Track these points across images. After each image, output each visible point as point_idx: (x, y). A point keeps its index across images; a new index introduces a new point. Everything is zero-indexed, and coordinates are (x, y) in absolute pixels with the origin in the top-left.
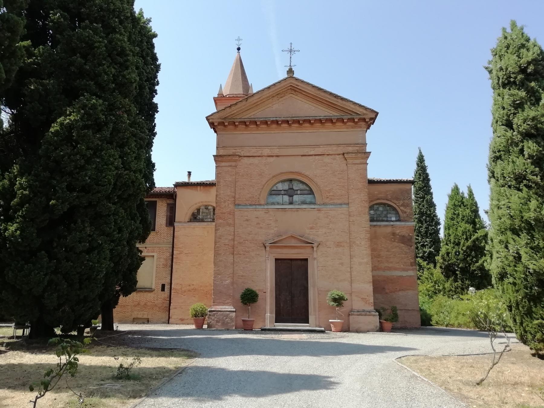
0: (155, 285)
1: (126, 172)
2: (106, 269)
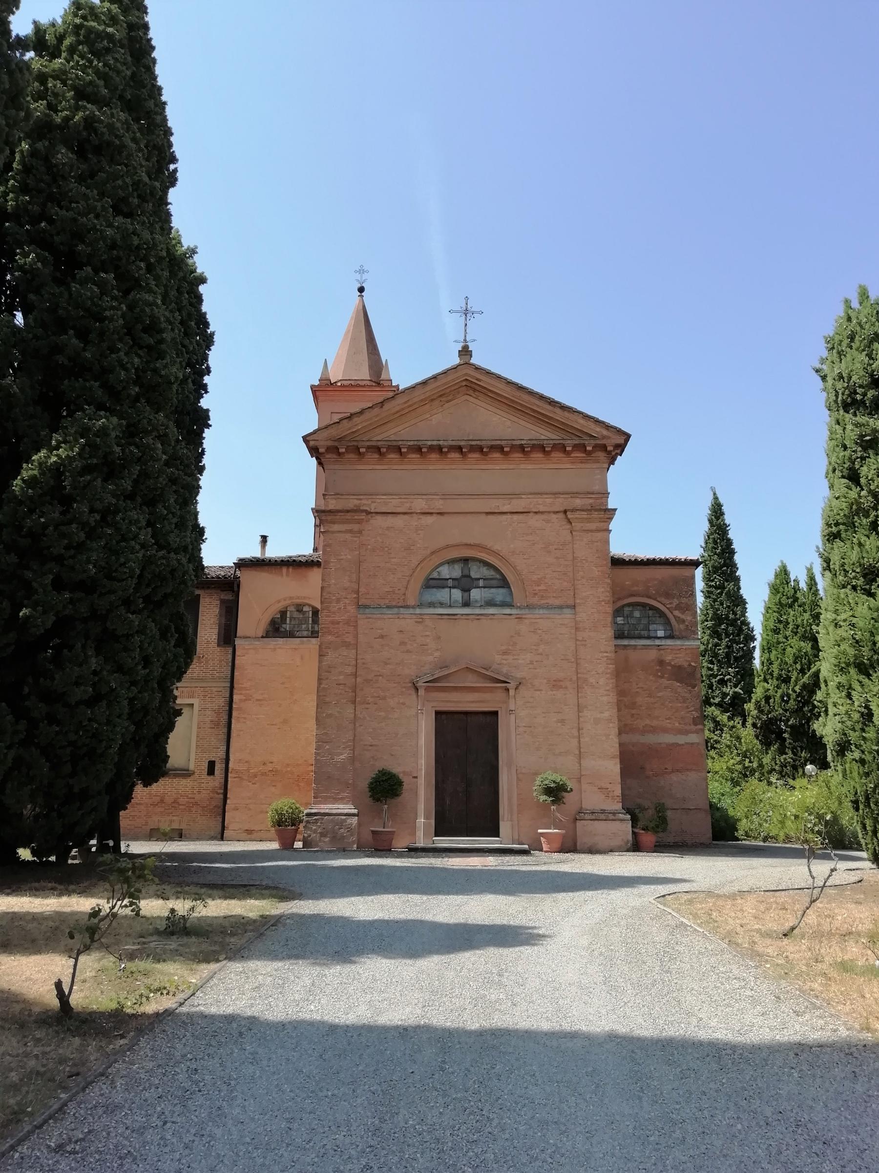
0: (195, 761)
1: (161, 553)
2: (122, 735)
